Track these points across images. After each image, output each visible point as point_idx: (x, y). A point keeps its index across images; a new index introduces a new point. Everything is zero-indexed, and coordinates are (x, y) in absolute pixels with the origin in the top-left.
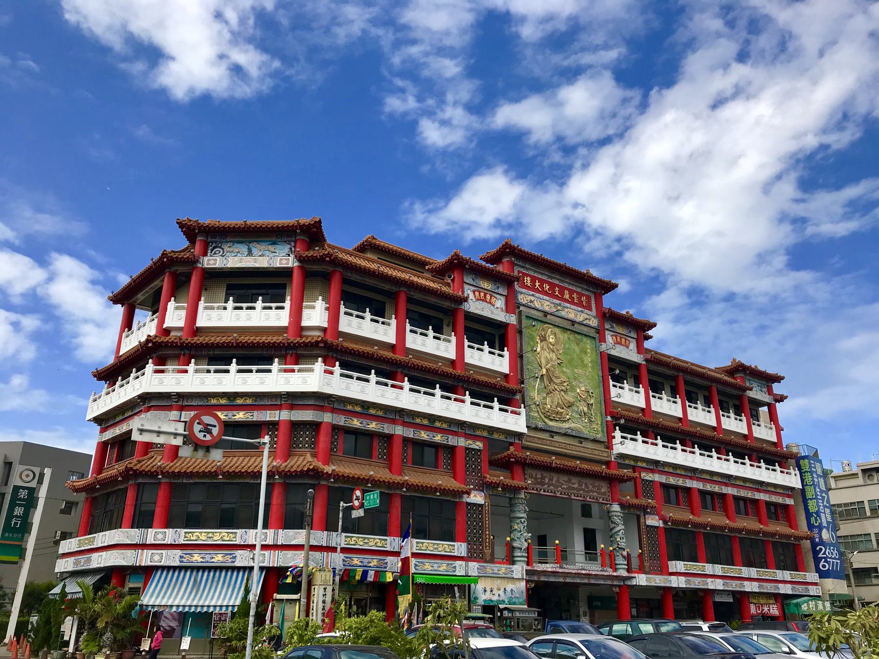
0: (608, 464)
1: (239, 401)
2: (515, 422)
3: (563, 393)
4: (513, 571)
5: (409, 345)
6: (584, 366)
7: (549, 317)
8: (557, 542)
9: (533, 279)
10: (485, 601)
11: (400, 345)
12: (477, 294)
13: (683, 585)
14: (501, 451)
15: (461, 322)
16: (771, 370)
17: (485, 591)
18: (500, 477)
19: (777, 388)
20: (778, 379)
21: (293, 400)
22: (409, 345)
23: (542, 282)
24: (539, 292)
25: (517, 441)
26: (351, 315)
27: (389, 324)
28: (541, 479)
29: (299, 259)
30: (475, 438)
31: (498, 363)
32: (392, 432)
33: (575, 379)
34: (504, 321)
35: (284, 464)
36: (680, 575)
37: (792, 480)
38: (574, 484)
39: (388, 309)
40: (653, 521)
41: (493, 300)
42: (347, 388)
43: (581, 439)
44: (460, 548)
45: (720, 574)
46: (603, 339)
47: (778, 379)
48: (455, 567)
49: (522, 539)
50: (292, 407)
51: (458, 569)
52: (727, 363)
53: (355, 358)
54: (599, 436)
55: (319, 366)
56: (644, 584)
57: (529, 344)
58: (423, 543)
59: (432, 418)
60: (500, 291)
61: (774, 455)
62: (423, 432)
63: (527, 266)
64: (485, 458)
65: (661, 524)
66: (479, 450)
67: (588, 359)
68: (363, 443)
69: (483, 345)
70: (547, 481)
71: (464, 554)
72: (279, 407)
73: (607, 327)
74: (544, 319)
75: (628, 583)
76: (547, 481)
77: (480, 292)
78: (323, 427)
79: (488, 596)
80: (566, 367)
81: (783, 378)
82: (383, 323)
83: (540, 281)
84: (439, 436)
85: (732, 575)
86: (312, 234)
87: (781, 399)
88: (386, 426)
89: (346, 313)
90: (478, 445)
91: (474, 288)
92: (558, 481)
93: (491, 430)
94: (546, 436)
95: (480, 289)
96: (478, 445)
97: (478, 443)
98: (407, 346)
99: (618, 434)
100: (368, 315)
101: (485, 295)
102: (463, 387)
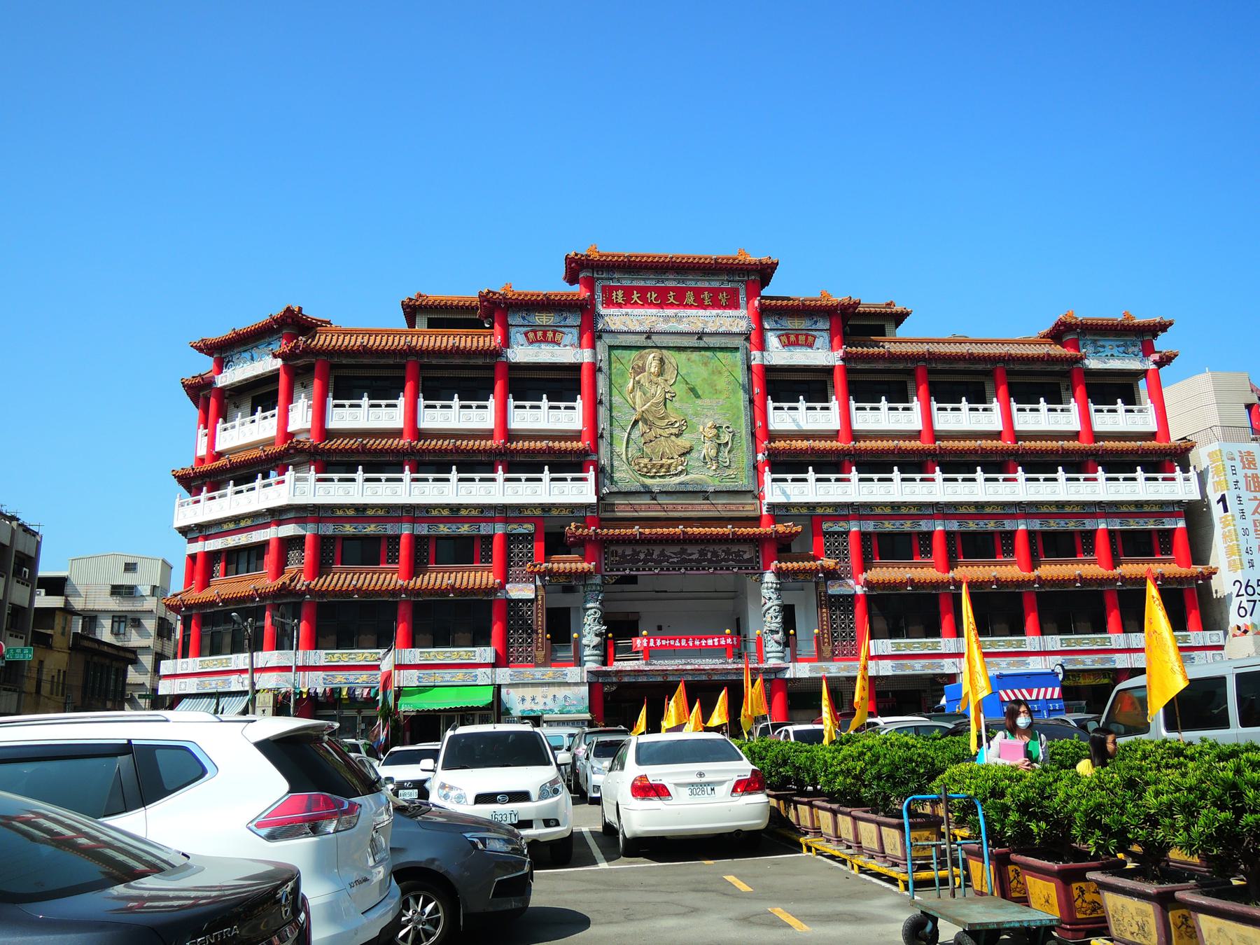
0: (756, 521)
1: (225, 527)
3: (673, 438)
5: (856, 426)
12: (531, 335)
14: (552, 531)
16: (1142, 317)
17: (523, 700)
19: (1162, 343)
21: (276, 515)
22: (856, 426)
27: (1068, 410)
29: (282, 356)
30: (521, 520)
31: (783, 419)
34: (825, 363)
35: (314, 583)
39: (989, 389)
41: (558, 336)
43: (704, 494)
44: (486, 654)
46: (762, 346)
49: (590, 632)
51: (480, 677)
52: (1047, 327)
53: (332, 455)
56: (806, 676)
60: (820, 325)
62: (441, 526)
66: (529, 534)
69: (798, 401)
70: (642, 556)
72: (266, 526)
73: (767, 326)
75: (780, 676)
77: (535, 332)
82: (985, 410)
83: (639, 289)
84: (373, 526)
85: (1095, 647)
86: (293, 324)
87: (1165, 360)
88: (389, 526)
94: (646, 500)
97: (526, 526)
98: (771, 428)
99: (768, 476)
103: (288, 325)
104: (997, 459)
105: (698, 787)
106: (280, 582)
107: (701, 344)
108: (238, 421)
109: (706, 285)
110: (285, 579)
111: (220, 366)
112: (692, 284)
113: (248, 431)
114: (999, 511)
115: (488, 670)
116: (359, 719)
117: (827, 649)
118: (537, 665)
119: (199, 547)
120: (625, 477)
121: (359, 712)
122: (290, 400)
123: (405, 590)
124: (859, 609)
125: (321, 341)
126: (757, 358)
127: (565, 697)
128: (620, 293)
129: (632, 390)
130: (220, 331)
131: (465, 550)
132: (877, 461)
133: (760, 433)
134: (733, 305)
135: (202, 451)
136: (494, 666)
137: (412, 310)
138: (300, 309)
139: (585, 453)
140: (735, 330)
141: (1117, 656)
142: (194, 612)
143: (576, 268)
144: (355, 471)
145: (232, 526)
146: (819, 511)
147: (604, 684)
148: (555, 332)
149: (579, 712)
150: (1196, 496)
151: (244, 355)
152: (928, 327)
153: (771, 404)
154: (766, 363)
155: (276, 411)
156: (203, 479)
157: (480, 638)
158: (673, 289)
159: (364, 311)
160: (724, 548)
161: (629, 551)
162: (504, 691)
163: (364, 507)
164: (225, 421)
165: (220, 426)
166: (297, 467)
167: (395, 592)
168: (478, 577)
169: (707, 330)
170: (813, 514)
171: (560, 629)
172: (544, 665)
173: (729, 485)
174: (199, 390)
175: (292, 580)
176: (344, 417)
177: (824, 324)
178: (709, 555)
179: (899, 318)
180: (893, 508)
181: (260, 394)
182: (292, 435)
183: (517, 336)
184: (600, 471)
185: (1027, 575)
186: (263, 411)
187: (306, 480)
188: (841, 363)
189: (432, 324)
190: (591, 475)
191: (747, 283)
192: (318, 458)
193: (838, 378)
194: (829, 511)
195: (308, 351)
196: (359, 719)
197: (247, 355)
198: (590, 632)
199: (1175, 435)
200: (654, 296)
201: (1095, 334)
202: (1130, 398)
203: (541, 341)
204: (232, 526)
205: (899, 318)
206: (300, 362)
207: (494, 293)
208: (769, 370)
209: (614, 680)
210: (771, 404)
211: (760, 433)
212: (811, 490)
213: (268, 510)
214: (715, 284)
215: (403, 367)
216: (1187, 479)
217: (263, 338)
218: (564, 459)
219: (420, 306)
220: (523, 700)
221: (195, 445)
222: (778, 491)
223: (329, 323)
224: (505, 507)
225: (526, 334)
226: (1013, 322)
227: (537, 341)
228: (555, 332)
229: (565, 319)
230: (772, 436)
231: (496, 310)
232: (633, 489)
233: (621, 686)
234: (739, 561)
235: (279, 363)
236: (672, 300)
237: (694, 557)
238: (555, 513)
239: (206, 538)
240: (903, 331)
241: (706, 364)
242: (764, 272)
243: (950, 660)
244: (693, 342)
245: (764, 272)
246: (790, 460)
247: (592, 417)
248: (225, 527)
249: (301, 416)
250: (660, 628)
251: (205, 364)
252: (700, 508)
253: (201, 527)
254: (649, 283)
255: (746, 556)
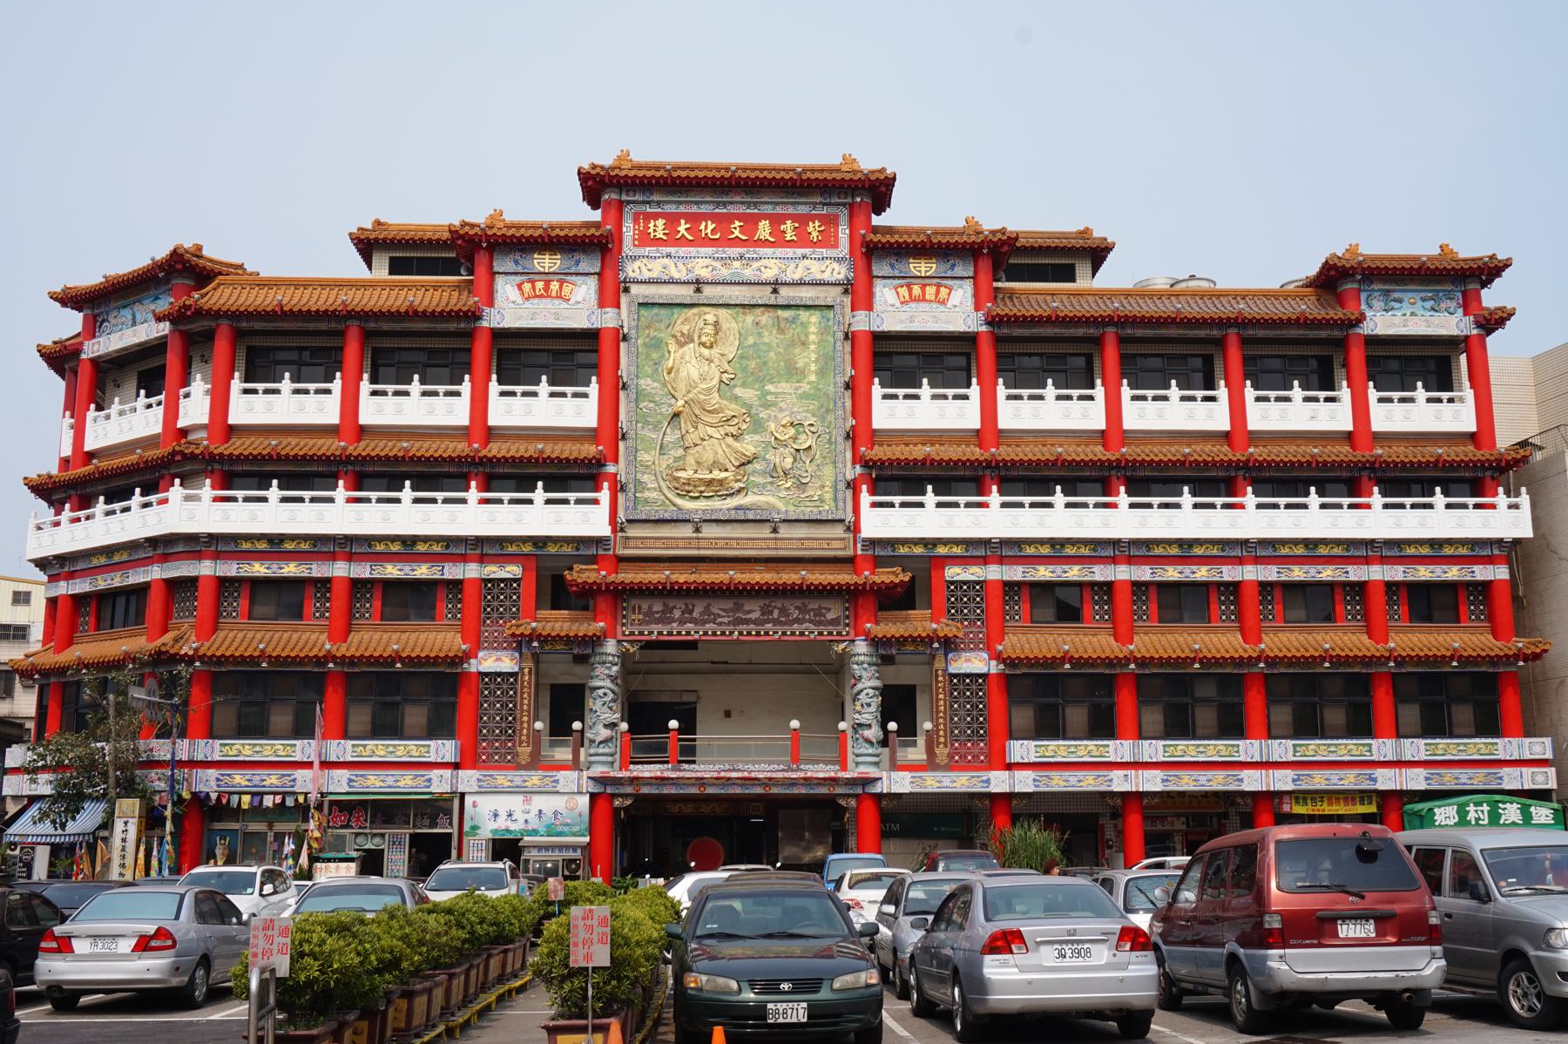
1: (95, 562)
2: (583, 518)
3: (730, 440)
4: (557, 781)
6: (793, 372)
7: (784, 291)
8: (795, 724)
9: (672, 220)
10: (494, 831)
11: (1237, 433)
12: (527, 287)
13: (1159, 787)
14: (554, 573)
15: (1357, 355)
16: (1469, 249)
18: (558, 622)
19: (1492, 297)
20: (1490, 271)
23: (695, 219)
24: (690, 243)
25: (601, 552)
26: (1390, 400)
28: (663, 612)
32: (1111, 578)
33: (767, 405)
36: (1034, 766)
37: (1505, 518)
38: (749, 612)
40: (974, 662)
42: (254, 519)
44: (445, 749)
45: (1423, 758)
47: (1490, 271)
48: (429, 780)
50: (482, 559)
54: (827, 510)
55: (176, 492)
57: (648, 355)
58: (364, 746)
59: (409, 541)
60: (960, 270)
61: (1471, 471)
63: (656, 198)
64: (528, 590)
65: (995, 668)
66: (515, 580)
67: (808, 359)
68: (1179, 602)
70: (677, 614)
71: (450, 758)
74: (696, 298)
76: (677, 614)
77: (533, 282)
78: (201, 585)
79: (502, 823)
80: (744, 385)
81: (1507, 264)
83: (690, 217)
86: (184, 269)
89: (1381, 400)
90: (513, 571)
91: (519, 279)
92: (707, 610)
93: (540, 542)
95: (532, 276)
96: (513, 571)
97: (510, 568)
99: (866, 498)
100: (1421, 393)
101: (547, 283)
102: (1493, 478)
103: (180, 273)
104: (1216, 473)
105: (1072, 941)
106: (158, 642)
107: (776, 300)
108: (115, 408)
109: (791, 210)
110: (168, 638)
111: (93, 328)
112: (768, 209)
113: (129, 422)
114: (1215, 552)
115: (447, 773)
116: (270, 837)
117: (942, 752)
118: (519, 767)
119: (63, 588)
120: (655, 495)
121: (270, 827)
122: (185, 381)
123: (330, 657)
124: (995, 686)
125: (218, 297)
126: (862, 322)
127: (556, 813)
128: (660, 222)
129: (686, 366)
130: (90, 277)
131: (411, 599)
132: (1032, 475)
133: (860, 433)
134: (828, 241)
135: (67, 451)
136: (456, 766)
137: (367, 246)
138: (199, 248)
139: (599, 462)
140: (827, 276)
141: (1245, 773)
142: (53, 680)
143: (595, 185)
144: (268, 487)
145: (103, 561)
146: (942, 550)
147: (613, 796)
148: (562, 282)
149: (574, 835)
150: (1526, 531)
151: (123, 312)
152: (1145, 264)
153: (877, 390)
154: (874, 328)
155: (162, 397)
156: (71, 488)
157: (437, 729)
158: (739, 217)
159: (298, 246)
160: (798, 603)
161: (658, 607)
162: (468, 800)
163: (280, 539)
164: (99, 408)
165: (92, 413)
166: (186, 481)
167: (321, 661)
168: (434, 638)
169: (784, 278)
170: (926, 560)
171: (566, 708)
172: (528, 767)
173: (808, 511)
174: (60, 358)
175: (176, 640)
176: (248, 408)
177: (964, 269)
178: (776, 614)
179: (1097, 254)
180: (1053, 546)
181: (147, 370)
182: (184, 432)
183: (506, 290)
184: (617, 488)
185: (1250, 651)
186: (147, 396)
187: (197, 498)
188: (984, 328)
189: (396, 267)
190: (604, 495)
191: (851, 207)
192: (217, 466)
193: (986, 351)
194: (957, 551)
195: (200, 313)
196: (270, 837)
197: (127, 313)
198: (603, 714)
199: (1505, 439)
200: (711, 226)
201: (1385, 282)
202: (1442, 380)
203: (541, 296)
204: (103, 561)
205: (1097, 254)
206: (195, 327)
207: (472, 226)
208: (878, 337)
209: (629, 790)
210: (877, 390)
211: (860, 433)
212: (927, 519)
213: (148, 540)
214: (803, 210)
215: (342, 334)
216: (1515, 506)
217: (147, 289)
218: (570, 473)
219: (376, 239)
220: (496, 815)
221: (49, 449)
222: (887, 521)
223: (241, 267)
224: (480, 541)
225: (519, 286)
226: (1264, 262)
227: (536, 296)
228: (562, 282)
229: (577, 263)
230: (875, 437)
231: (471, 250)
232: (667, 516)
233: (639, 799)
234: (820, 623)
235: (165, 328)
236: (737, 233)
237: (753, 616)
238: (552, 549)
239: (71, 576)
240: (1111, 276)
241: (781, 330)
242: (878, 190)
243: (1121, 773)
244: (764, 295)
245: (878, 190)
246: (898, 475)
247: (609, 408)
248: (95, 562)
249: (195, 408)
250: (728, 714)
251: (71, 322)
252: (755, 541)
253: (62, 559)
254: (705, 209)
255: (830, 616)
